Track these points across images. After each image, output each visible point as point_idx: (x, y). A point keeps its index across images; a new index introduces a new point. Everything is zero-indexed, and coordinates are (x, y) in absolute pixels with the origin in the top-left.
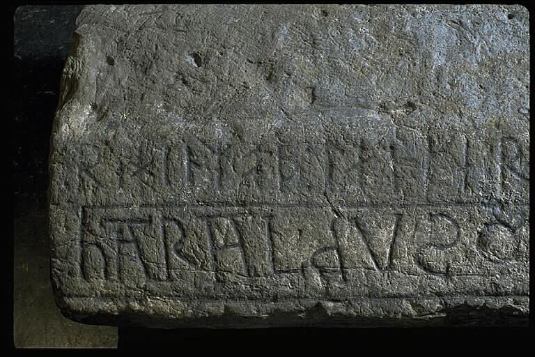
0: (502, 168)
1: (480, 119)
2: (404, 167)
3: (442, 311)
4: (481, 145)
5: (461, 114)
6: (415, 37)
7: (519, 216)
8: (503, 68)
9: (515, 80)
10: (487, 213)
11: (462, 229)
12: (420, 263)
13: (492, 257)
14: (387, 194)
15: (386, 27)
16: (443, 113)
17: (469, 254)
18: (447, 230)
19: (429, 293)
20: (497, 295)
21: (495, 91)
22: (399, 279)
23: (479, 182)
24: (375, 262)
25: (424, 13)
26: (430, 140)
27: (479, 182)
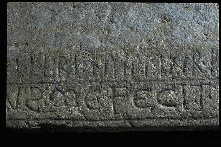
0: (59, 68)
1: (51, 48)
2: (21, 68)
3: (38, 126)
4: (51, 59)
5: (44, 47)
6: (35, 16)
7: (65, 88)
8: (65, 28)
9: (69, 33)
10: (52, 87)
11: (43, 93)
12: (28, 106)
13: (56, 104)
14: (15, 79)
15: (24, 13)
16: (38, 47)
17: (47, 103)
18: (38, 93)
19: (32, 118)
20: (59, 119)
21: (60, 38)
22: (20, 113)
23: (50, 74)
24: (11, 106)
25: (40, 7)
26: (32, 58)
27: (50, 74)
